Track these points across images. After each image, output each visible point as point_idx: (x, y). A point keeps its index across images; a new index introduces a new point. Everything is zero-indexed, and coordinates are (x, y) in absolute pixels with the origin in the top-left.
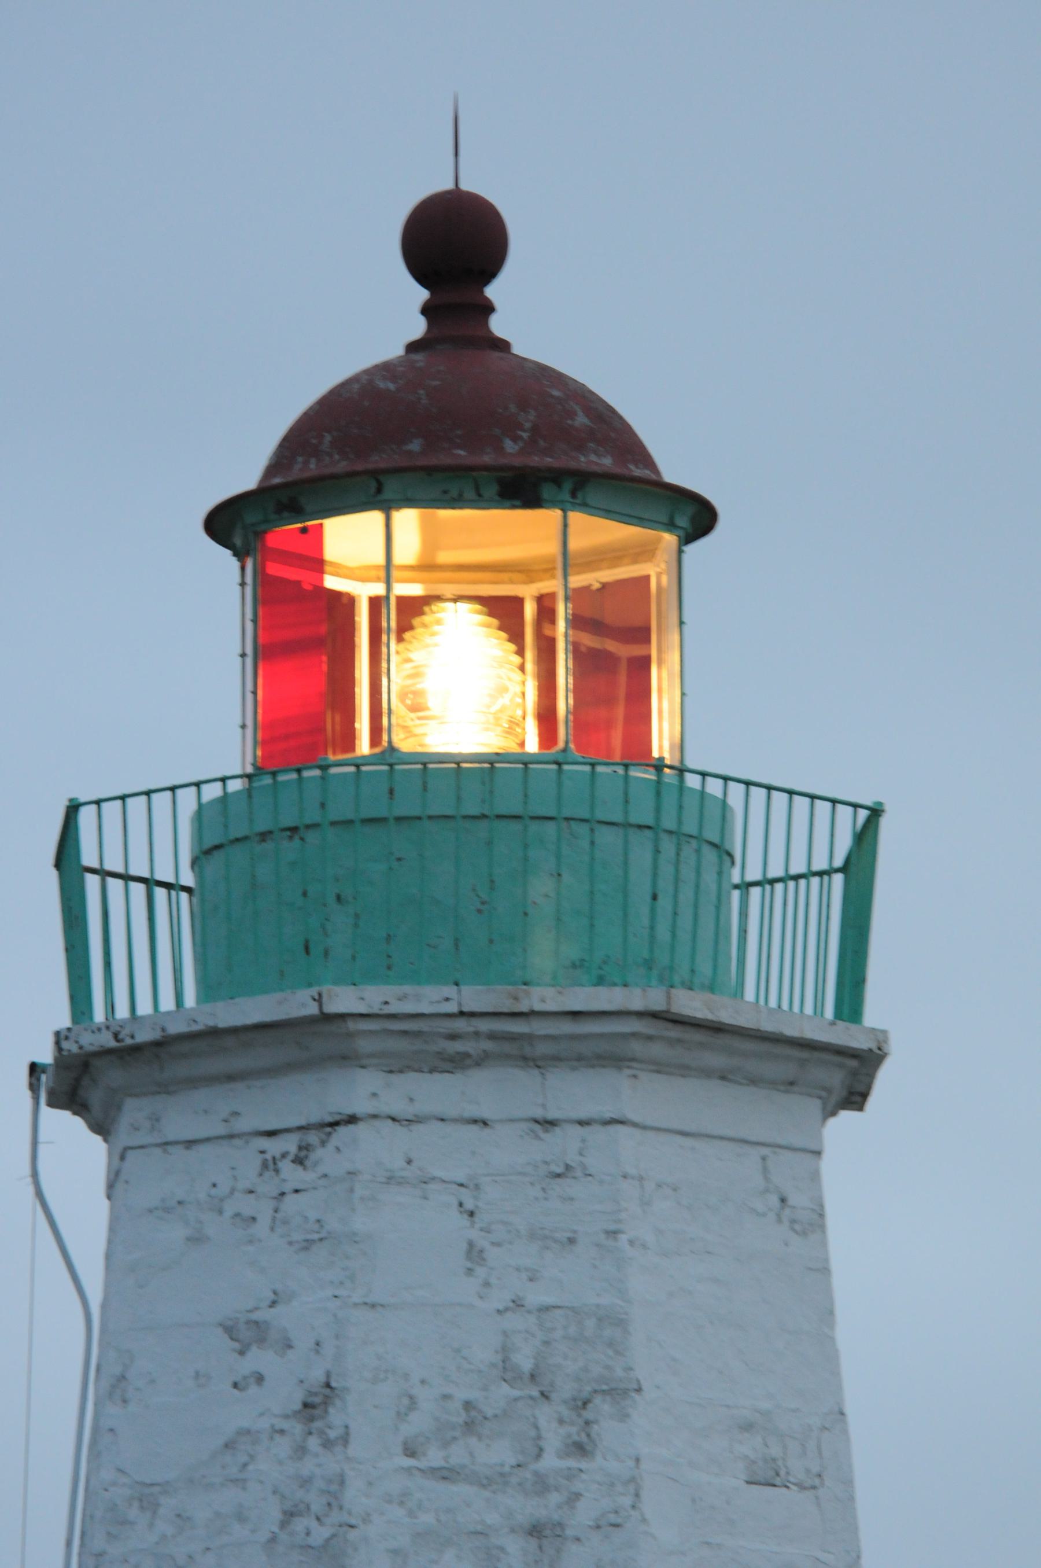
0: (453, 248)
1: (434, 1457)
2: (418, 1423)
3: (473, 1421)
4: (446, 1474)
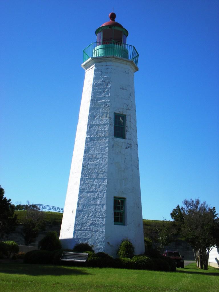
0: (113, 16)
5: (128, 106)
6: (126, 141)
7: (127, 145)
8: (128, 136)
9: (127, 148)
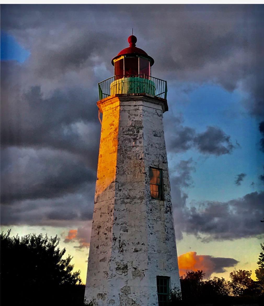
1: (126, 133)
2: (124, 130)
3: (129, 130)
4: (127, 135)
5: (164, 158)
6: (165, 203)
7: (166, 209)
8: (166, 197)
9: (166, 213)
